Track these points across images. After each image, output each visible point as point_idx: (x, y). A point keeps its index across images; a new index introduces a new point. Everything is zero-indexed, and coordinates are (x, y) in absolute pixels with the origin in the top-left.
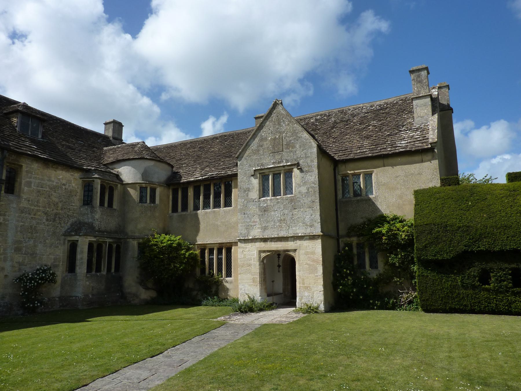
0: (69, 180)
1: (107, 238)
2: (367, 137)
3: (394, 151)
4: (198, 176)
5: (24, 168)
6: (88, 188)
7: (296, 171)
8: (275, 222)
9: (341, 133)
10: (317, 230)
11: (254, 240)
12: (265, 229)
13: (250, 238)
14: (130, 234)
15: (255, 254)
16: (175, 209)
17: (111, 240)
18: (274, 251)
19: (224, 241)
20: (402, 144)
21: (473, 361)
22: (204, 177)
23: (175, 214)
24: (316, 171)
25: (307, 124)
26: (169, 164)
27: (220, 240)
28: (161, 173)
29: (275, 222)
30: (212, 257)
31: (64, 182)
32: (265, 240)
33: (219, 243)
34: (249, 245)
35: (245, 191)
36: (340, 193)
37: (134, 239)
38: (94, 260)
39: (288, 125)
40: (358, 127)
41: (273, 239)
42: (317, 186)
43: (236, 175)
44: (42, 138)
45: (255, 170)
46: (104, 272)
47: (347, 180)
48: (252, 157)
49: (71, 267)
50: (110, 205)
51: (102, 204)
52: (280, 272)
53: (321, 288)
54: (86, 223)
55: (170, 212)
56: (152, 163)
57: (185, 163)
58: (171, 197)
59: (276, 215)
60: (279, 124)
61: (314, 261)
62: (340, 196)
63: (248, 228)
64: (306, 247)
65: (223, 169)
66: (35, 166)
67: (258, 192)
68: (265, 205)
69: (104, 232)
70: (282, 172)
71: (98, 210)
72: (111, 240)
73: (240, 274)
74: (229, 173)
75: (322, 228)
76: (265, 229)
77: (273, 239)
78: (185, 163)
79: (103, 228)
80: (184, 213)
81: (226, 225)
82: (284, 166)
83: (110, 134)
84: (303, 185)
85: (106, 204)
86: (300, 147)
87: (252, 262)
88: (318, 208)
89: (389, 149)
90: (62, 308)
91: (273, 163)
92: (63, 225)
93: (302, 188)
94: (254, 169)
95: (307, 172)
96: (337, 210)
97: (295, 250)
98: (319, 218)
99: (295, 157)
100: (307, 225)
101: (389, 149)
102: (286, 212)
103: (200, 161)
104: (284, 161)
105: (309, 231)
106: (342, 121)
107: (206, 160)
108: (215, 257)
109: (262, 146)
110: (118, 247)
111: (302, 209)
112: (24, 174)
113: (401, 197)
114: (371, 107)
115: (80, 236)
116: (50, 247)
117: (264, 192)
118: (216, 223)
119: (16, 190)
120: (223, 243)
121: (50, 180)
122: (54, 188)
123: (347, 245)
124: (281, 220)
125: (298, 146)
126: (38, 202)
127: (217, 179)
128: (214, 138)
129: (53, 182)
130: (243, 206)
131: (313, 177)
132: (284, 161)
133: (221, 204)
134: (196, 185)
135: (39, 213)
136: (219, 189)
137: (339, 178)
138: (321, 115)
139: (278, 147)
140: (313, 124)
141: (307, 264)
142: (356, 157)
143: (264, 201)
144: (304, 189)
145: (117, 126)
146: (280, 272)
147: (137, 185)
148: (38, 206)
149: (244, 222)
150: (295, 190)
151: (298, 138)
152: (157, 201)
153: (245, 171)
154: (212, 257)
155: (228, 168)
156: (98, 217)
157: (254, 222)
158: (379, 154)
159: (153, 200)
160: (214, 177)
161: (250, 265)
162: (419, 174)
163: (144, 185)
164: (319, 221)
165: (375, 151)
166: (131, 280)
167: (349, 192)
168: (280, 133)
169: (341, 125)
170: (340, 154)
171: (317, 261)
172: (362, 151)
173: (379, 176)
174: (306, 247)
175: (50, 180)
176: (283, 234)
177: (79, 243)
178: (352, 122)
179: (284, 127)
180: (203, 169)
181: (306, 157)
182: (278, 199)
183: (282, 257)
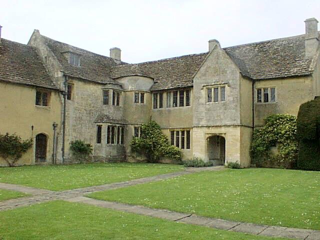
4: (170, 86)
6: (106, 93)
12: (208, 120)
16: (155, 107)
20: (294, 71)
21: (98, 93)
26: (151, 78)
31: (94, 92)
32: (208, 127)
34: (199, 130)
43: (192, 86)
45: (204, 86)
46: (115, 144)
50: (118, 104)
51: (114, 104)
52: (217, 142)
55: (152, 108)
58: (153, 98)
63: (200, 120)
66: (80, 83)
78: (161, 76)
80: (161, 109)
85: (116, 104)
91: (215, 82)
93: (230, 98)
94: (203, 85)
95: (233, 88)
97: (225, 134)
105: (235, 123)
108: (180, 137)
110: (123, 129)
112: (75, 88)
122: (89, 96)
131: (236, 92)
137: (256, 91)
141: (232, 142)
146: (217, 142)
148: (82, 106)
152: (145, 100)
153: (198, 81)
156: (110, 111)
159: (142, 101)
163: (137, 92)
171: (237, 140)
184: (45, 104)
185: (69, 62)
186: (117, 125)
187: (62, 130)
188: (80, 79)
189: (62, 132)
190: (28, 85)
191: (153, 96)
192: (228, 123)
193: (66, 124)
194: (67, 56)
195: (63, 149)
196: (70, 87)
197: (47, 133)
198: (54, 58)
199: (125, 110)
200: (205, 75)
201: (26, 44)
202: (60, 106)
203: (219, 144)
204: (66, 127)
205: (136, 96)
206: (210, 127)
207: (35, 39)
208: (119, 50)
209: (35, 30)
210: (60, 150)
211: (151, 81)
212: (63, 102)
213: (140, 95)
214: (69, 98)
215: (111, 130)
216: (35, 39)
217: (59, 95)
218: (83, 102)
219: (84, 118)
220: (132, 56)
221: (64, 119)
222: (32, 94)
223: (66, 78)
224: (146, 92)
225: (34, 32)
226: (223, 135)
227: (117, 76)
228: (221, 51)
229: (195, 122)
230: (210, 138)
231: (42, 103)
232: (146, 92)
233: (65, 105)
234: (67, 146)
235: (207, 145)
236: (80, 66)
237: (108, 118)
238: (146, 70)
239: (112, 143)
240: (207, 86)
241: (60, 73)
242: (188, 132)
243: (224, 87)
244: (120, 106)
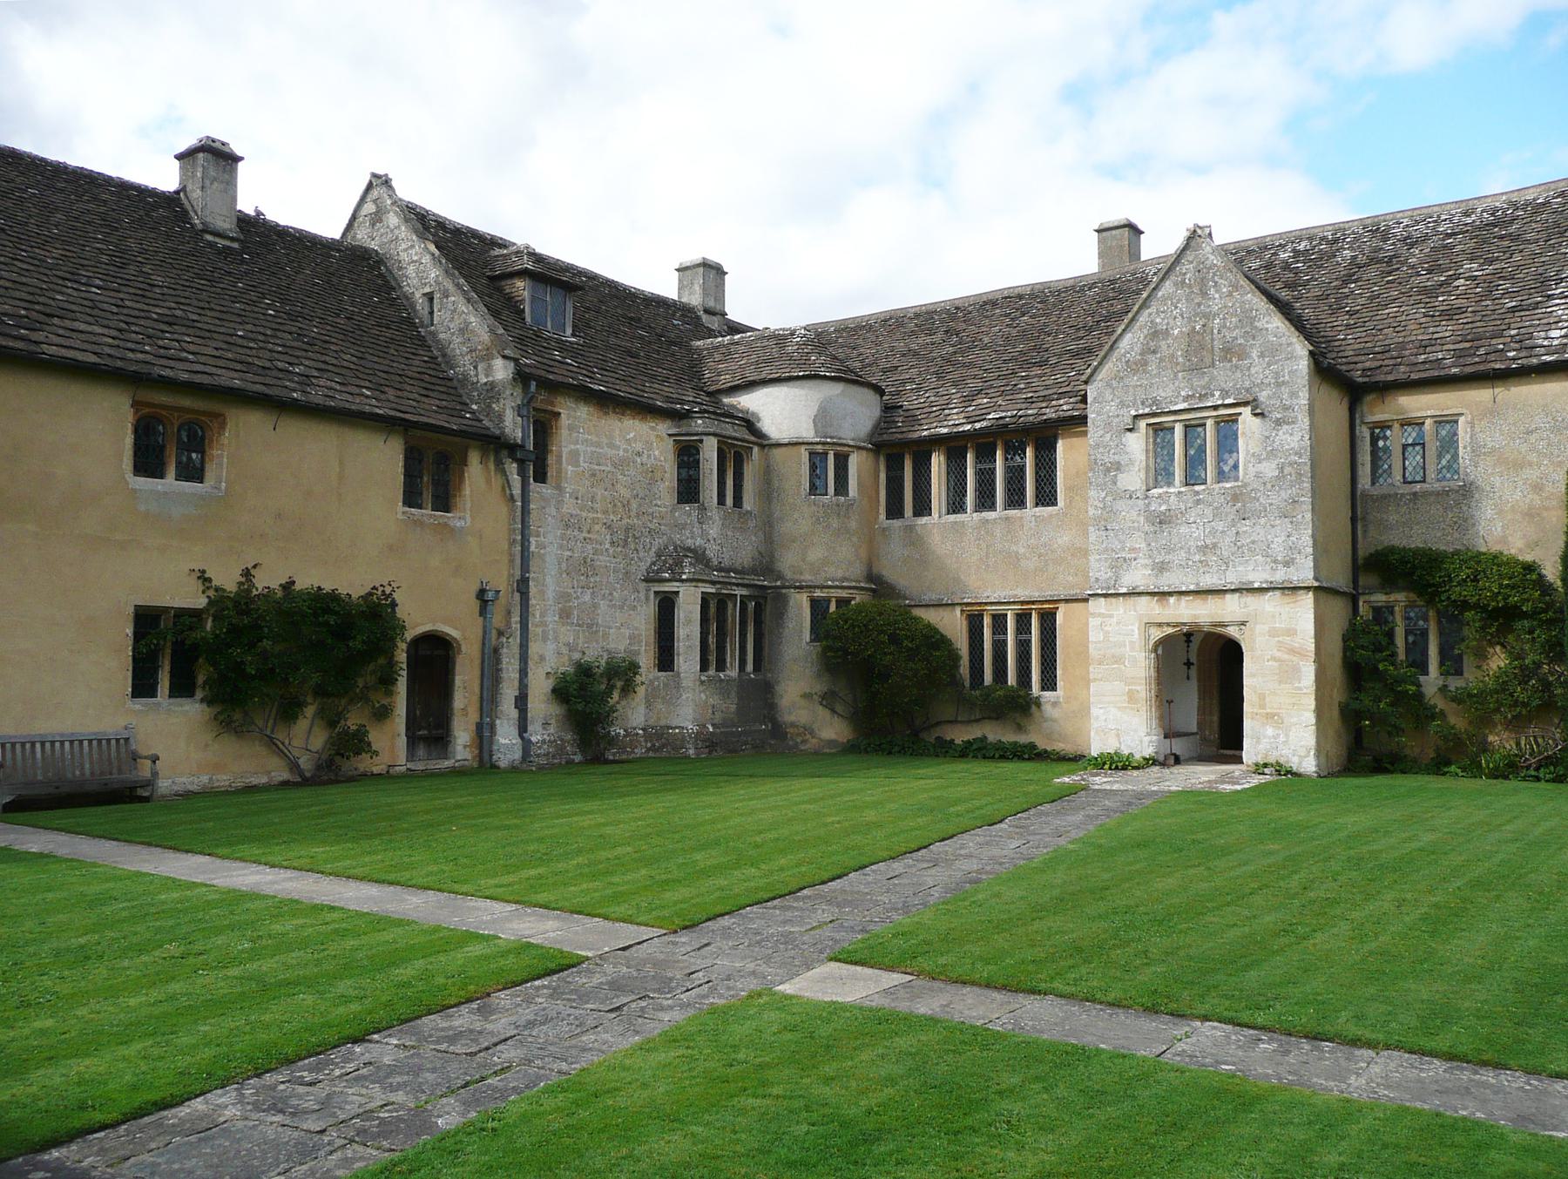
0: (645, 443)
1: (737, 585)
2: (1449, 314)
3: (1525, 361)
4: (955, 421)
5: (564, 420)
6: (687, 455)
7: (1247, 421)
8: (1189, 552)
9: (1371, 298)
10: (1304, 572)
11: (1133, 594)
12: (1161, 568)
13: (1124, 590)
14: (789, 575)
15: (1134, 632)
16: (895, 510)
17: (745, 592)
19: (1036, 595)
22: (978, 425)
23: (896, 523)
24: (1304, 422)
25: (1269, 266)
27: (1023, 593)
28: (857, 414)
29: (1189, 552)
30: (1002, 637)
31: (639, 446)
34: (1119, 608)
36: (1365, 471)
37: (801, 587)
38: (712, 640)
39: (1230, 294)
40: (1424, 280)
42: (1306, 459)
44: (573, 335)
45: (1136, 417)
46: (732, 672)
47: (1385, 438)
48: (1127, 381)
49: (666, 659)
50: (738, 501)
51: (721, 500)
52: (1205, 675)
53: (1310, 718)
54: (689, 549)
55: (883, 516)
56: (836, 389)
57: (911, 380)
58: (883, 476)
59: (1192, 532)
60: (1204, 294)
62: (1364, 481)
63: (1119, 564)
65: (1030, 401)
67: (1143, 475)
68: (1163, 508)
69: (728, 570)
70: (1209, 423)
71: (714, 512)
72: (745, 592)
74: (1050, 414)
75: (1316, 567)
76: (1161, 568)
78: (911, 380)
79: (726, 563)
82: (1215, 408)
83: (695, 299)
84: (1267, 458)
85: (729, 500)
86: (1262, 355)
88: (1309, 516)
89: (1511, 354)
90: (651, 754)
91: (1186, 398)
92: (641, 554)
93: (1265, 464)
94: (1133, 413)
95: (1279, 422)
96: (1354, 520)
97: (1243, 623)
98: (1310, 543)
99: (1247, 384)
100: (1275, 561)
101: (1511, 354)
102: (1220, 526)
103: (955, 376)
104: (1217, 394)
106: (1373, 261)
107: (975, 371)
109: (1154, 352)
111: (1263, 521)
112: (564, 432)
113: (1537, 488)
114: (1466, 214)
115: (682, 581)
116: (621, 608)
117: (1160, 474)
118: (1014, 548)
119: (552, 472)
121: (611, 445)
122: (621, 464)
123: (1377, 611)
125: (1255, 354)
126: (593, 499)
127: (1015, 431)
128: (985, 303)
129: (618, 448)
131: (1295, 437)
132: (1217, 394)
133: (994, 489)
134: (955, 446)
135: (597, 527)
136: (1021, 456)
138: (1310, 239)
139: (1201, 352)
140: (1286, 266)
141: (1274, 659)
142: (1414, 376)
143: (1160, 496)
144: (1269, 469)
145: (712, 274)
146: (1205, 675)
147: (803, 448)
150: (1245, 469)
151: (1253, 333)
153: (1108, 398)
154: (1002, 637)
155: (1045, 398)
156: (711, 531)
157: (1133, 550)
158: (1482, 367)
160: (1006, 425)
161: (1118, 660)
163: (819, 448)
164: (1310, 550)
165: (1469, 360)
166: (798, 689)
167: (1389, 472)
168: (1206, 316)
169: (1372, 272)
170: (1368, 365)
172: (1432, 357)
173: (1477, 429)
175: (611, 445)
176: (1209, 581)
177: (681, 599)
178: (1404, 263)
179: (1216, 301)
180: (968, 400)
181: (1278, 385)
182: (1197, 493)
183: (1195, 645)
184: (444, 502)
185: (528, 319)
186: (739, 592)
187: (516, 618)
188: (585, 394)
189: (516, 626)
190: (798, 378)
191: (882, 468)
192: (1258, 578)
193: (533, 589)
194: (521, 288)
195: (521, 702)
196: (543, 427)
197: (454, 633)
198: (469, 301)
199: (768, 526)
200: (1139, 366)
201: (337, 236)
202: (504, 510)
203: (1193, 672)
204: (532, 602)
205: (813, 467)
206: (1170, 594)
207: (377, 218)
208: (1134, 230)
209: (374, 175)
210: (508, 706)
211: (870, 396)
212: (517, 492)
213: (831, 458)
214: (541, 477)
215: (714, 610)
216: (377, 218)
217: (499, 464)
218: (600, 492)
219: (602, 560)
220: (771, 295)
221: (525, 567)
222: (383, 459)
223: (526, 386)
224: (859, 448)
225: (370, 187)
226: (1232, 632)
227: (726, 380)
228: (1215, 260)
229: (1099, 571)
230: (1165, 642)
231: (427, 497)
232: (859, 448)
233: (525, 511)
234: (540, 687)
235: (1153, 673)
236: (573, 335)
237: (700, 557)
238: (830, 354)
239: (718, 670)
240: (1154, 415)
241: (498, 363)
242: (1048, 619)
243: (1233, 419)
244: (747, 506)
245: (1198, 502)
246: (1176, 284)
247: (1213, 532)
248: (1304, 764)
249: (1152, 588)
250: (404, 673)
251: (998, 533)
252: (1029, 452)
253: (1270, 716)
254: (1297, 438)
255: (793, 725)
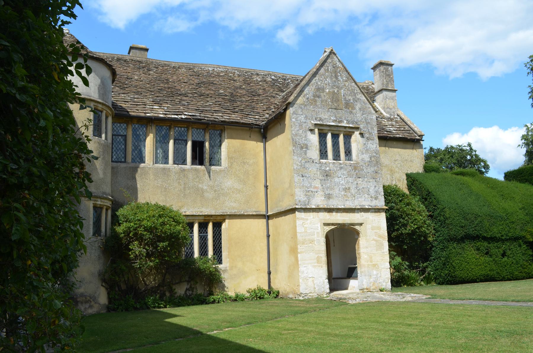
11: (318, 210)
12: (329, 197)
18: (339, 224)
19: (213, 213)
32: (330, 210)
33: (205, 216)
34: (311, 216)
35: (302, 148)
41: (338, 210)
48: (308, 107)
61: (380, 236)
64: (372, 221)
68: (328, 169)
73: (301, 253)
77: (338, 210)
81: (215, 191)
82: (345, 127)
87: (315, 237)
95: (368, 139)
97: (361, 224)
100: (371, 197)
104: (345, 121)
111: (366, 179)
118: (200, 186)
120: (211, 216)
124: (346, 189)
130: (301, 166)
141: (374, 240)
149: (303, 186)
153: (299, 120)
157: (315, 187)
161: (312, 241)
162: (411, 161)
163: (100, 107)
174: (372, 221)
176: (349, 204)
182: (340, 164)
200: (313, 102)
245: (341, 168)
246: (325, 70)
247: (348, 182)
248: (388, 286)
249: (326, 206)
250: (399, 299)
251: (190, 176)
252: (171, 143)
253: (374, 265)
254: (375, 146)
255: (82, 295)
